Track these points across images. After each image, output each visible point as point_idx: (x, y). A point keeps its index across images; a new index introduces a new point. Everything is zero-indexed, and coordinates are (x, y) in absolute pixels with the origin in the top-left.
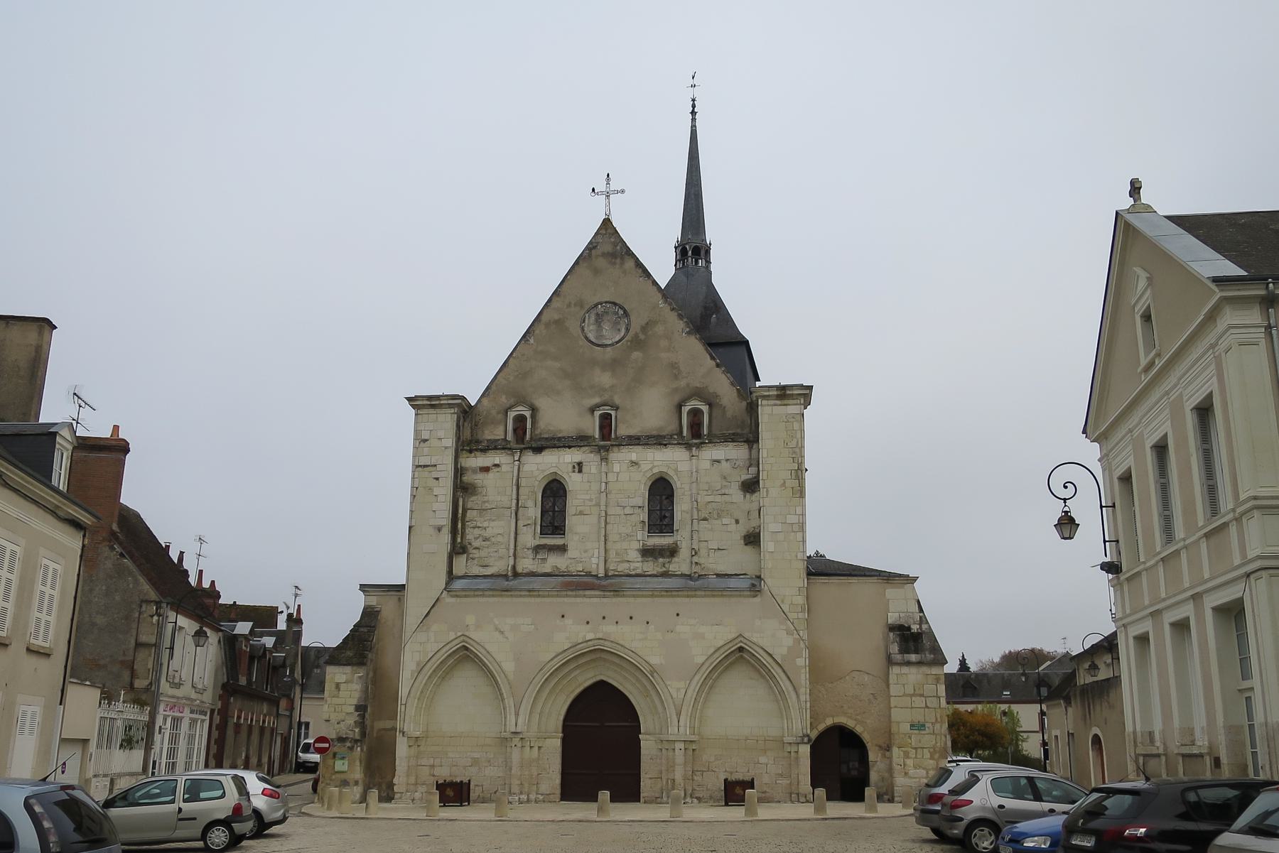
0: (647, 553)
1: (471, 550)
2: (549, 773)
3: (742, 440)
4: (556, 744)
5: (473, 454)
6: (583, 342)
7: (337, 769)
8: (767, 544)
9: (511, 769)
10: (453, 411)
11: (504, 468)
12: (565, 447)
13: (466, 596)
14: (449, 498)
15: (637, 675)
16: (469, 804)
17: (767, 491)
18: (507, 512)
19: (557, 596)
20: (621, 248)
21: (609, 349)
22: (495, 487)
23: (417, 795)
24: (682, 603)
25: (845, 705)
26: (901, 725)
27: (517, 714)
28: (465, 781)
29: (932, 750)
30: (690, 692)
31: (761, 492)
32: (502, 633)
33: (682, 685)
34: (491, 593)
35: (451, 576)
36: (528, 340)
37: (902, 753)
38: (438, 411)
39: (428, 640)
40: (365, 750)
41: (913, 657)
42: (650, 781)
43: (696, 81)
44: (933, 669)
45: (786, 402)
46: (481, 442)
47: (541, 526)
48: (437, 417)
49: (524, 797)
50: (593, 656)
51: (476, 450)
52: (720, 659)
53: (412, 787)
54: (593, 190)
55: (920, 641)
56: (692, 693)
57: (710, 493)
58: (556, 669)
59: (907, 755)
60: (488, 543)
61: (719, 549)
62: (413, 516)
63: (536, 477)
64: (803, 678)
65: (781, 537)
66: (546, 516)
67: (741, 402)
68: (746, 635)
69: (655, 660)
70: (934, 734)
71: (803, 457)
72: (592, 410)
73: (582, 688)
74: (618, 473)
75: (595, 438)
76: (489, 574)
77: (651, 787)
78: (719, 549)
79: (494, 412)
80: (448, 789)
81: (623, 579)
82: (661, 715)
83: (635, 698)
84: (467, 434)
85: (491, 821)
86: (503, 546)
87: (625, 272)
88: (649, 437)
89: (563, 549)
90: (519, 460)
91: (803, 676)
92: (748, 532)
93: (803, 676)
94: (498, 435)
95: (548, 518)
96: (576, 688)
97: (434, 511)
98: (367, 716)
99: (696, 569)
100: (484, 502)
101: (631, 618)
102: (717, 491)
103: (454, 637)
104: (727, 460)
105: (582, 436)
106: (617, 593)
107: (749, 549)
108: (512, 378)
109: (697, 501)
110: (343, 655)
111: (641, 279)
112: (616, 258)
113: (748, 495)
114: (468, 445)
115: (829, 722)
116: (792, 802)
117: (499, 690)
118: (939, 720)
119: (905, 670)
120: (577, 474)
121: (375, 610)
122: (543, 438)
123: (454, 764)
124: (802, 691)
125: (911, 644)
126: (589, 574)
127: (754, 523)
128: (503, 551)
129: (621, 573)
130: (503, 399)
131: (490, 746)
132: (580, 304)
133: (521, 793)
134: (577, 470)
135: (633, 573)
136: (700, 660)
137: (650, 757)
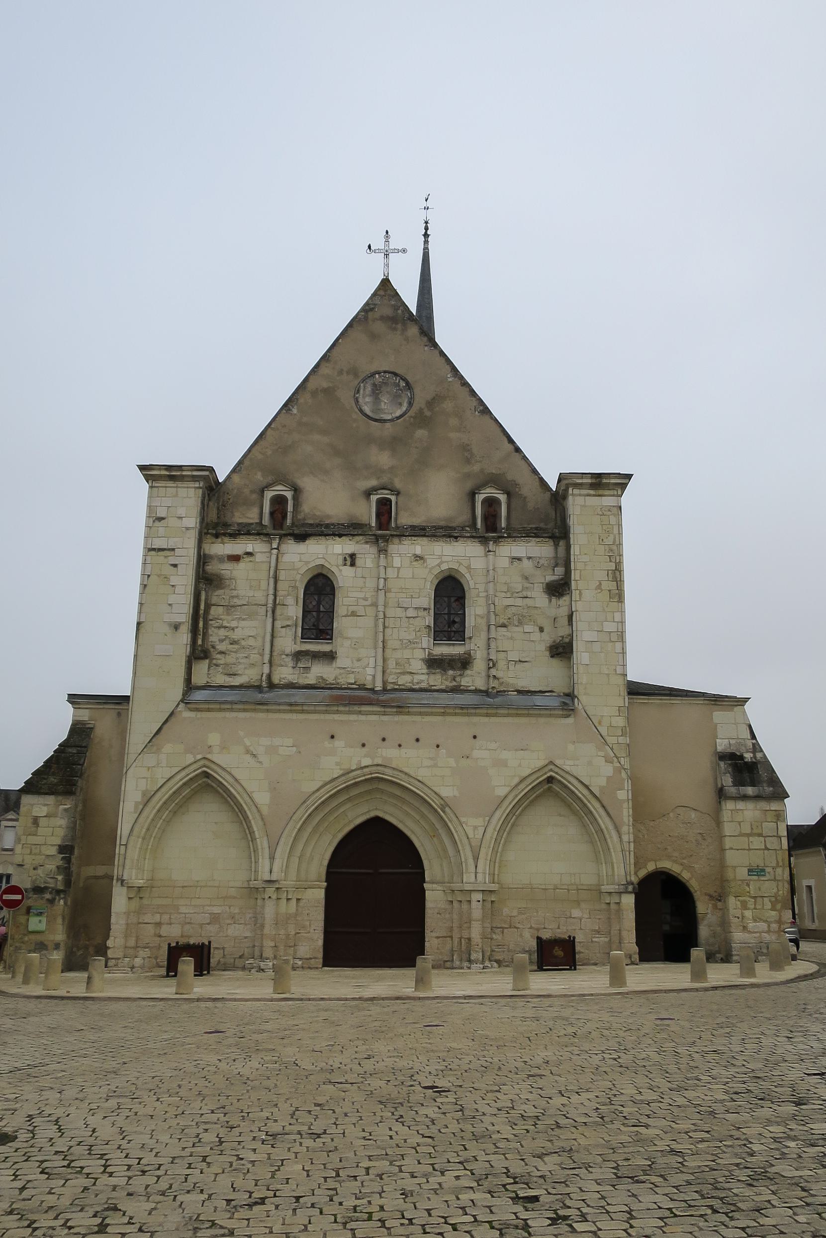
0: (434, 663)
2: (309, 933)
3: (546, 535)
4: (318, 895)
5: (219, 540)
7: (31, 927)
8: (581, 655)
10: (197, 485)
11: (259, 558)
12: (334, 535)
13: (209, 710)
14: (190, 589)
15: (422, 809)
16: (209, 973)
17: (580, 594)
19: (326, 712)
20: (403, 312)
21: (388, 425)
23: (138, 961)
24: (480, 723)
25: (668, 847)
26: (738, 870)
27: (272, 858)
29: (773, 899)
30: (490, 830)
31: (573, 595)
32: (254, 756)
33: (479, 822)
34: (241, 706)
35: (189, 686)
36: (290, 410)
37: (738, 903)
38: (179, 484)
40: (69, 903)
41: (750, 790)
42: (436, 941)
43: (429, 204)
44: (772, 804)
45: (601, 492)
46: (230, 525)
47: (303, 629)
48: (177, 492)
50: (368, 787)
51: (224, 534)
54: (369, 247)
55: (755, 772)
56: (491, 832)
57: (509, 595)
58: (323, 802)
59: (744, 906)
60: (236, 646)
63: (298, 569)
64: (626, 814)
65: (596, 647)
67: (545, 493)
68: (558, 762)
69: (445, 792)
70: (775, 880)
71: (621, 555)
72: (368, 494)
73: (351, 826)
74: (399, 569)
75: (371, 527)
76: (237, 684)
77: (438, 949)
78: (520, 661)
79: (246, 491)
81: (405, 695)
83: (418, 837)
84: (213, 516)
86: (256, 651)
87: (407, 339)
88: (436, 528)
92: (554, 642)
94: (250, 518)
96: (345, 825)
97: (170, 605)
98: (74, 860)
99: (493, 683)
100: (233, 597)
101: (418, 740)
102: (517, 593)
103: (193, 760)
104: (529, 558)
105: (355, 524)
106: (400, 710)
107: (555, 662)
108: (269, 452)
110: (45, 781)
111: (426, 348)
112: (397, 324)
113: (554, 600)
114: (214, 528)
115: (651, 867)
118: (781, 864)
119: (741, 805)
121: (87, 726)
122: (308, 524)
123: (188, 920)
124: (625, 829)
125: (746, 775)
126: (362, 687)
127: (564, 631)
128: (255, 657)
129: (403, 687)
130: (259, 476)
131: (234, 898)
132: (354, 372)
134: (348, 563)
135: (417, 687)
136: (502, 792)
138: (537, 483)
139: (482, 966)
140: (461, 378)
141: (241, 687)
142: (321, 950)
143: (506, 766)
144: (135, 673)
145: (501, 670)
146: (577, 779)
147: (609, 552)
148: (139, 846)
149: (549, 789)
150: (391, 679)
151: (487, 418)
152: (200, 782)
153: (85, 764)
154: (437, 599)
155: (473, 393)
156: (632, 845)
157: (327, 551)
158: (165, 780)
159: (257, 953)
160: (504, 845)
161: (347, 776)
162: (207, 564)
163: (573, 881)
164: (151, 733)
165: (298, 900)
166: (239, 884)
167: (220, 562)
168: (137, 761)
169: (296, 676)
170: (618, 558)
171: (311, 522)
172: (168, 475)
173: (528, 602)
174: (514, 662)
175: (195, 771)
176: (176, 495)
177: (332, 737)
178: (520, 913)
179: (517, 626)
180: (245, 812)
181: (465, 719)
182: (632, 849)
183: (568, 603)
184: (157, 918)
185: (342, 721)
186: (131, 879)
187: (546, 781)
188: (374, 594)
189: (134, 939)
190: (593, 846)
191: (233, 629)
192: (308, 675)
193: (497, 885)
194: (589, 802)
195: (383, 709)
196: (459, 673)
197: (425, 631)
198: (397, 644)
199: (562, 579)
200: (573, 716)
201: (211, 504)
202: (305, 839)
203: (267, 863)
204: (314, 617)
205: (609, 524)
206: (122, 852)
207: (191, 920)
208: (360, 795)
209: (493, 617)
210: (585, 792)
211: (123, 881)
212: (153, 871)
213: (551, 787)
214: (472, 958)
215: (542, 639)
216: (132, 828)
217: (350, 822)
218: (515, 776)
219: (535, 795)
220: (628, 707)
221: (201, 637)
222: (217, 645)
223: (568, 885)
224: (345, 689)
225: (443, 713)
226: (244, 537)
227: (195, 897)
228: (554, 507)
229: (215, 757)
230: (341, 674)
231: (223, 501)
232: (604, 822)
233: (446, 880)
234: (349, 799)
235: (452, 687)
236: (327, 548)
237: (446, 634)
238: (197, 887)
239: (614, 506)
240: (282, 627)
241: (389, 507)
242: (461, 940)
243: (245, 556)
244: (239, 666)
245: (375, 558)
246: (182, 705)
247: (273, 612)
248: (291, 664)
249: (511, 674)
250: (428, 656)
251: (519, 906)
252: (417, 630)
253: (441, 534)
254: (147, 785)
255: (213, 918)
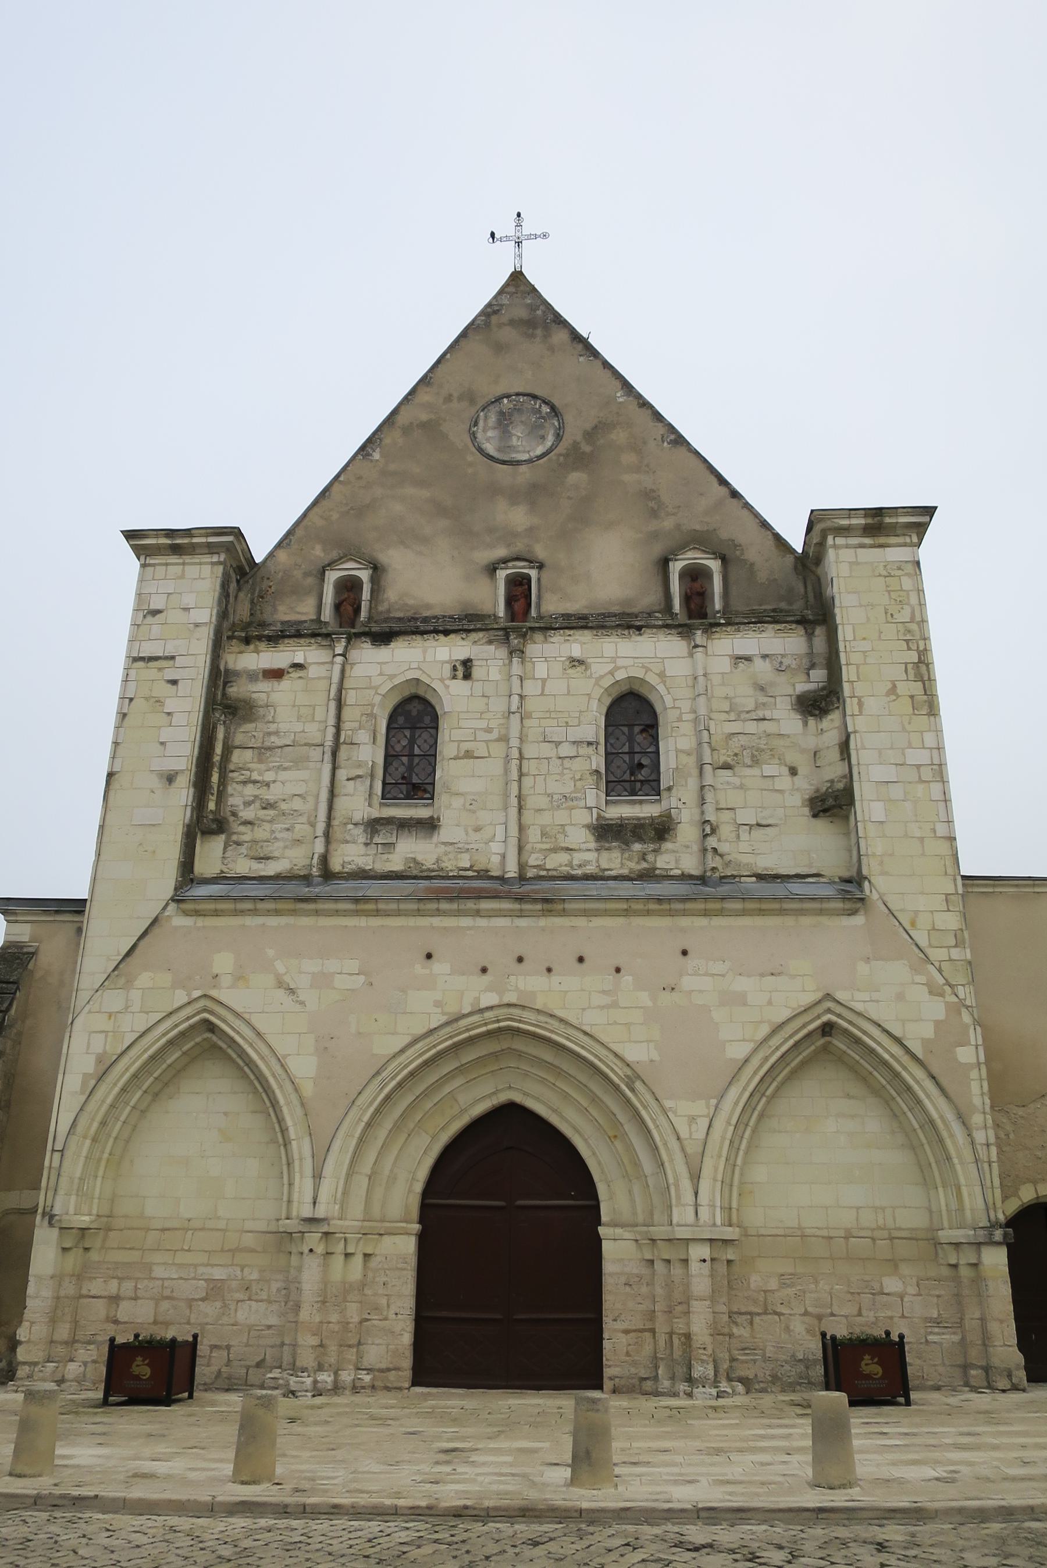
1: (236, 827)
2: (386, 1319)
5: (252, 647)
6: (473, 456)
9: (297, 1307)
11: (313, 671)
12: (436, 632)
13: (216, 913)
14: (196, 718)
16: (191, 1397)
17: (860, 704)
18: (315, 754)
19: (419, 913)
21: (523, 468)
22: (294, 706)
27: (318, 1176)
28: (184, 1335)
30: (719, 1124)
32: (292, 991)
33: (700, 1108)
34: (270, 905)
36: (369, 455)
38: (187, 559)
39: (127, 1008)
42: (623, 1339)
45: (882, 540)
47: (384, 784)
48: (183, 570)
49: (326, 1378)
50: (493, 1046)
51: (260, 638)
52: (784, 1049)
53: (60, 1350)
54: (493, 235)
57: (732, 716)
58: (412, 1074)
61: (759, 825)
62: (119, 753)
63: (376, 688)
65: (896, 792)
66: (395, 764)
67: (784, 556)
68: (840, 996)
69: (634, 1053)
71: (926, 639)
72: (492, 569)
74: (544, 681)
75: (496, 617)
76: (272, 873)
77: (628, 1354)
78: (759, 825)
79: (298, 574)
80: (139, 1359)
82: (651, 1181)
83: (586, 1140)
85: (212, 1509)
86: (304, 819)
87: (552, 349)
89: (430, 825)
90: (344, 655)
91: (975, 1088)
92: (817, 791)
93: (975, 1088)
94: (299, 613)
95: (399, 769)
96: (454, 1118)
97: (162, 743)
100: (269, 734)
101: (581, 960)
102: (748, 712)
103: (186, 1000)
104: (765, 657)
105: (470, 615)
107: (821, 825)
108: (335, 516)
109: (708, 730)
111: (581, 359)
112: (535, 328)
113: (812, 721)
114: (242, 630)
116: (975, 1389)
117: (279, 1122)
120: (442, 798)
121: (25, 950)
122: (394, 618)
123: (167, 1293)
124: (977, 1119)
126: (484, 875)
127: (833, 770)
128: (302, 829)
129: (555, 873)
131: (253, 1251)
132: (469, 397)
133: (320, 1368)
134: (460, 673)
135: (579, 872)
136: (738, 1051)
137: (623, 1280)
138: (770, 542)
139: (714, 1391)
140: (639, 396)
141: (277, 877)
142: (409, 1354)
143: (745, 1004)
144: (98, 854)
145: (726, 841)
146: (879, 1026)
147: (905, 635)
148: (84, 1153)
149: (825, 1049)
150: (533, 860)
151: (682, 450)
152: (198, 1040)
153: (13, 1011)
154: (610, 729)
155: (658, 417)
156: (994, 1150)
157: (425, 658)
158: (138, 1034)
159: (287, 1358)
160: (747, 1152)
161: (455, 1026)
162: (229, 684)
163: (881, 1222)
164: (118, 955)
165: (367, 1256)
166: (262, 1226)
167: (251, 681)
168: (91, 1003)
169: (370, 859)
170: (921, 644)
171: (399, 614)
172: (170, 544)
173: (769, 727)
174: (747, 828)
175: (188, 1018)
176: (182, 577)
177: (429, 956)
178: (783, 1285)
179: (749, 766)
180: (273, 1092)
181: (665, 922)
182: (994, 1157)
183: (837, 723)
184: (113, 1287)
185: (445, 928)
186: (67, 1214)
187: (820, 1031)
188: (502, 721)
189: (68, 1326)
190: (916, 1154)
191: (268, 785)
192: (390, 856)
193: (737, 1229)
194: (905, 1068)
195: (517, 906)
196: (652, 846)
197: (591, 780)
198: (543, 802)
199: (823, 689)
200: (862, 912)
201: (241, 595)
202: (379, 1143)
203: (308, 1184)
204: (403, 764)
205: (902, 590)
206: (56, 1163)
207: (172, 1291)
208: (480, 1061)
209: (707, 750)
210: (896, 1050)
211: (52, 1217)
212: (113, 1201)
213: (830, 1042)
214: (695, 1374)
215: (796, 787)
216: (75, 1120)
217: (463, 1111)
218: (761, 1022)
219: (800, 1057)
220: (963, 895)
221: (214, 798)
222: (241, 810)
223: (873, 1230)
224: (454, 877)
225: (626, 910)
226: (291, 641)
227: (183, 1250)
228: (800, 577)
229: (223, 995)
230: (446, 854)
231: (261, 590)
232: (937, 1106)
233: (640, 1219)
234: (460, 1070)
235: (639, 871)
236: (425, 652)
237: (627, 785)
238: (187, 1230)
239: (906, 562)
240: (348, 780)
241: (526, 587)
242: (671, 1337)
243: (290, 670)
244: (276, 844)
245: (504, 665)
246: (172, 906)
247: (334, 754)
248: (362, 839)
249: (743, 847)
250: (597, 820)
251: (782, 1271)
252: (578, 777)
253: (613, 624)
254: (105, 1044)
255: (213, 1289)
